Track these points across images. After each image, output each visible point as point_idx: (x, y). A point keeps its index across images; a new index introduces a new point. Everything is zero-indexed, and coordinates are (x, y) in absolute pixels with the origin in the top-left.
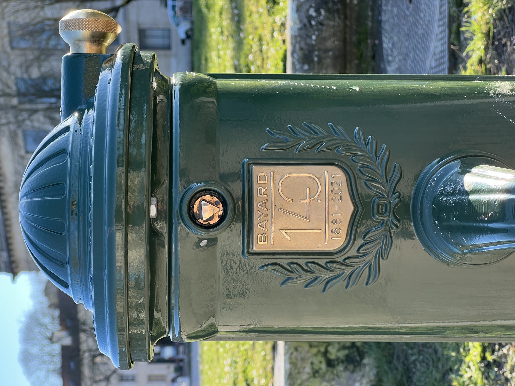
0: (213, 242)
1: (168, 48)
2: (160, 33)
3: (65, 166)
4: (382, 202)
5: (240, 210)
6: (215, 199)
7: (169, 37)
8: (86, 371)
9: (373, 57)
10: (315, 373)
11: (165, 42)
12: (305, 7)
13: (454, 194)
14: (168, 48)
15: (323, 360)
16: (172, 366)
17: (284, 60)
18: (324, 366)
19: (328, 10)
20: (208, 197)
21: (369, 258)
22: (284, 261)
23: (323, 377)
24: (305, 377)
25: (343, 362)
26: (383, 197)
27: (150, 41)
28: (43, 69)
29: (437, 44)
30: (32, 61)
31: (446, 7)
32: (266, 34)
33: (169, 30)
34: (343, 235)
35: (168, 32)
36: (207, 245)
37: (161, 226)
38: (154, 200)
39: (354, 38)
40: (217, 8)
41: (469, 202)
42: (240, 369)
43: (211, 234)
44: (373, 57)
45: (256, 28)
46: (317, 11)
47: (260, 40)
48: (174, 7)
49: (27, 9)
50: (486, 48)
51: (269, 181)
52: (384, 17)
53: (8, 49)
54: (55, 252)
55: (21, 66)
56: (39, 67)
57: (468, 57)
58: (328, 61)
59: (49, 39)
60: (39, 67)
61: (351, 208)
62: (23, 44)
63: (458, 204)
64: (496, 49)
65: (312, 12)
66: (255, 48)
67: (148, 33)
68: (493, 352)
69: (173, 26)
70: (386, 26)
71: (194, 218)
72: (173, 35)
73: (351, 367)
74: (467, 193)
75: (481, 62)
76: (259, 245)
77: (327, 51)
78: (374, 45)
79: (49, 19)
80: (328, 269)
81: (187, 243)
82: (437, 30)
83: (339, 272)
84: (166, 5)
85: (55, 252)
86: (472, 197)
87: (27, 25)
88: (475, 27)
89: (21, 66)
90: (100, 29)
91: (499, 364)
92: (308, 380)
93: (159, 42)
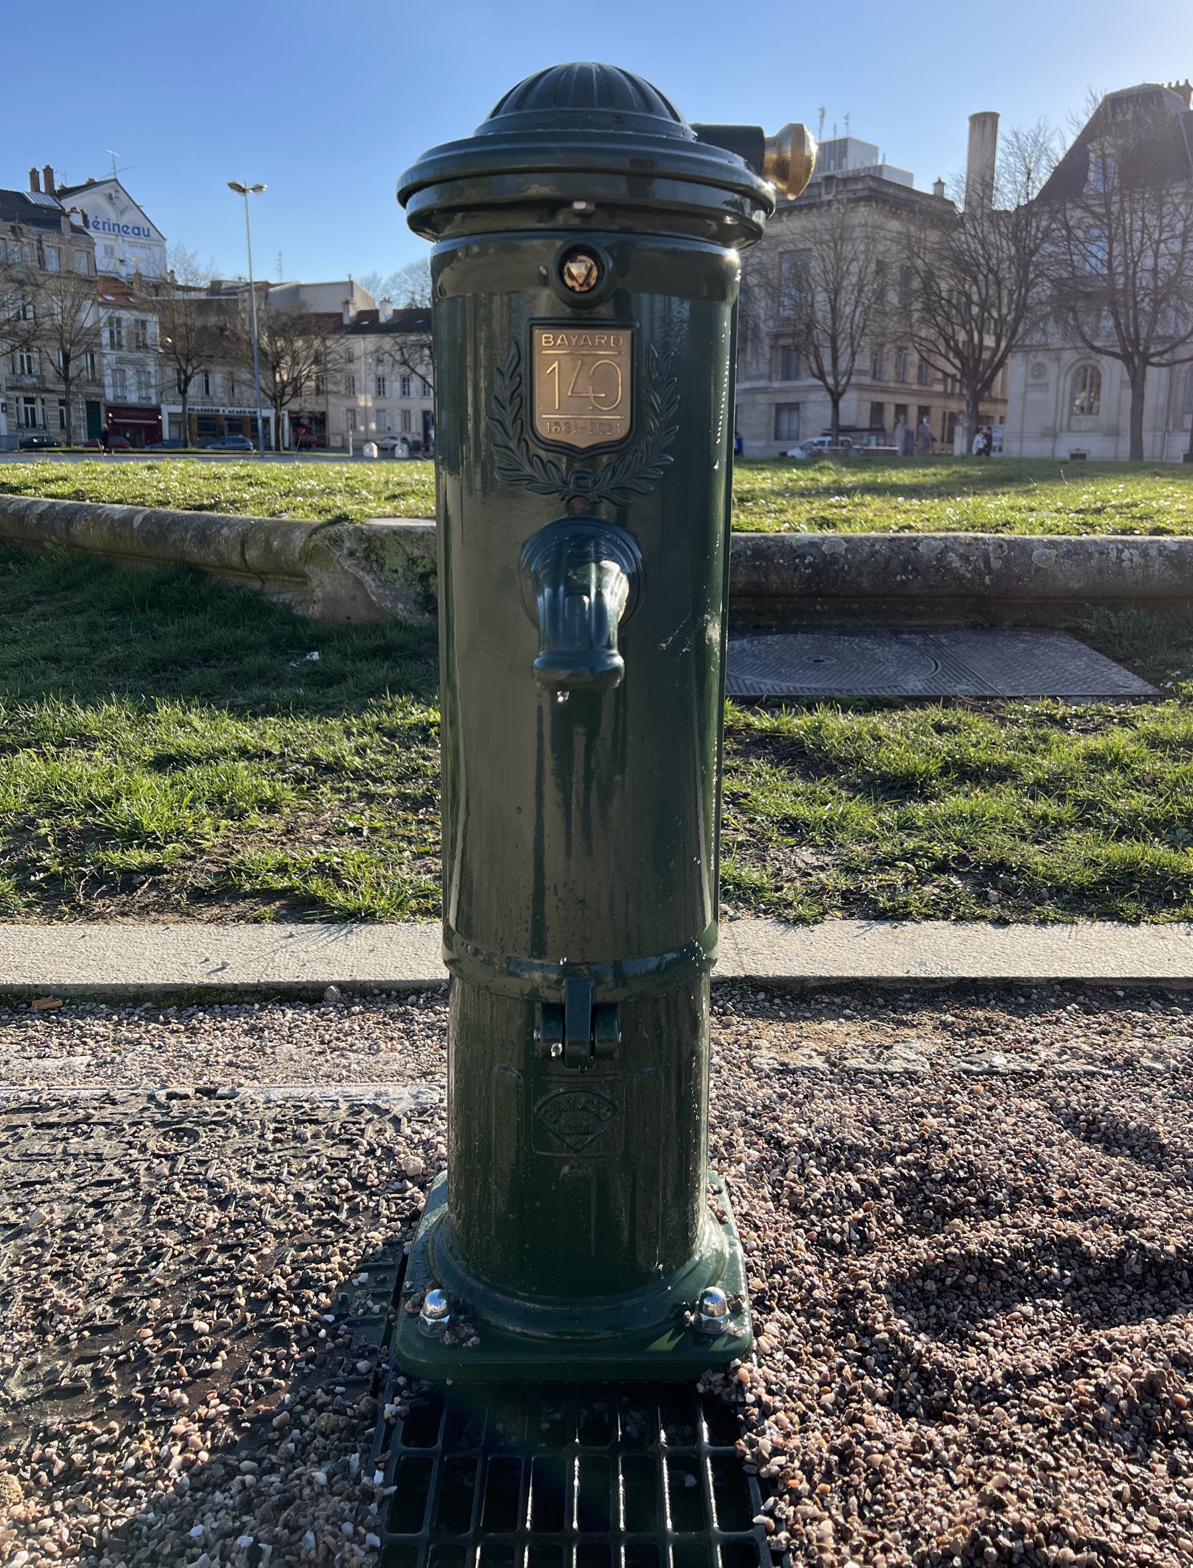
0: (544, 281)
1: (777, 438)
2: (794, 428)
3: (633, 108)
4: (590, 483)
5: (580, 313)
6: (593, 282)
7: (789, 439)
8: (413, 338)
9: (757, 627)
10: (413, 561)
11: (785, 435)
12: (814, 552)
13: (597, 552)
14: (777, 438)
15: (428, 569)
16: (420, 439)
17: (758, 531)
18: (420, 570)
19: (810, 577)
20: (595, 273)
21: (528, 470)
22: (523, 368)
23: (408, 569)
24: (408, 549)
25: (426, 591)
26: (595, 483)
27: (785, 416)
28: (756, 289)
29: (768, 686)
30: (767, 276)
31: (808, 693)
32: (789, 516)
33: (797, 438)
34: (553, 436)
35: (794, 437)
36: (540, 274)
37: (560, 219)
38: (592, 208)
39: (779, 607)
40: (818, 476)
41: (588, 563)
42: (416, 488)
43: (554, 276)
44: (757, 627)
45: (794, 508)
46: (810, 565)
47: (781, 511)
48: (822, 443)
49: (825, 272)
50: (762, 730)
51: (611, 351)
52: (800, 637)
53: (781, 250)
54: (532, 97)
55: (761, 263)
56: (759, 286)
57: (754, 714)
58: (755, 577)
59: (791, 297)
60: (759, 286)
61: (583, 446)
62: (785, 266)
63: (587, 554)
64: (762, 740)
65: (809, 559)
66: (773, 507)
67: (795, 414)
68: (438, 734)
69: (802, 443)
70: (790, 638)
71: (569, 255)
72: (790, 443)
73: (420, 600)
74: (597, 562)
75: (748, 725)
76: (544, 338)
77: (766, 575)
78: (770, 627)
79: (813, 297)
80: (514, 421)
81: (541, 252)
82: (784, 685)
83: (511, 432)
84: (824, 435)
85: (532, 97)
86: (593, 566)
87: (808, 273)
88: (785, 719)
89: (761, 263)
90: (792, 171)
91: (426, 740)
92: (405, 552)
93: (784, 427)
